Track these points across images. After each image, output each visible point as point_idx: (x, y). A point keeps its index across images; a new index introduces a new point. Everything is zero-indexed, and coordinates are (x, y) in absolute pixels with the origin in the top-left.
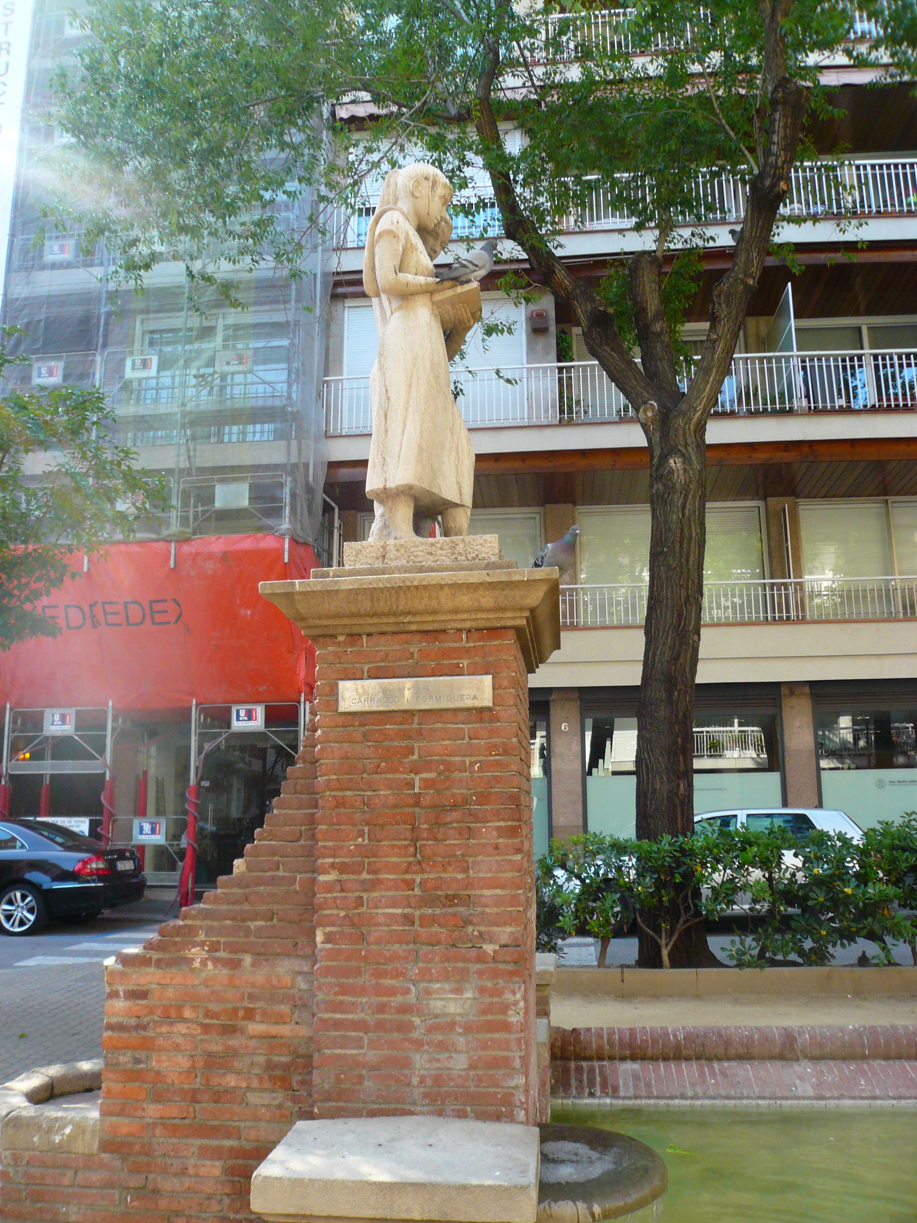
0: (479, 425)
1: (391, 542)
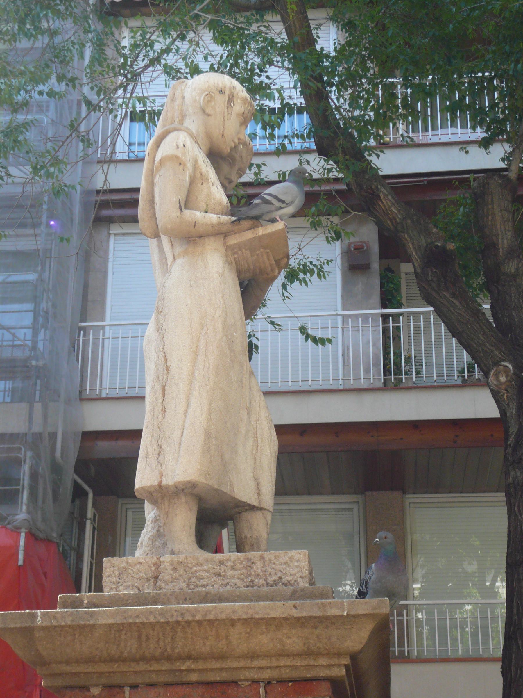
0: (280, 387)
1: (167, 558)
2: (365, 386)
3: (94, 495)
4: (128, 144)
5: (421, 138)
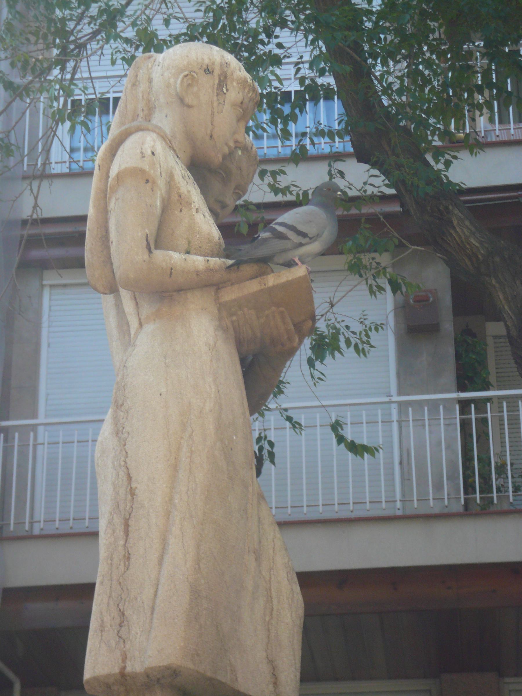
0: (306, 513)
2: (437, 510)
3: (23, 686)
4: (68, 150)
5: (512, 132)
